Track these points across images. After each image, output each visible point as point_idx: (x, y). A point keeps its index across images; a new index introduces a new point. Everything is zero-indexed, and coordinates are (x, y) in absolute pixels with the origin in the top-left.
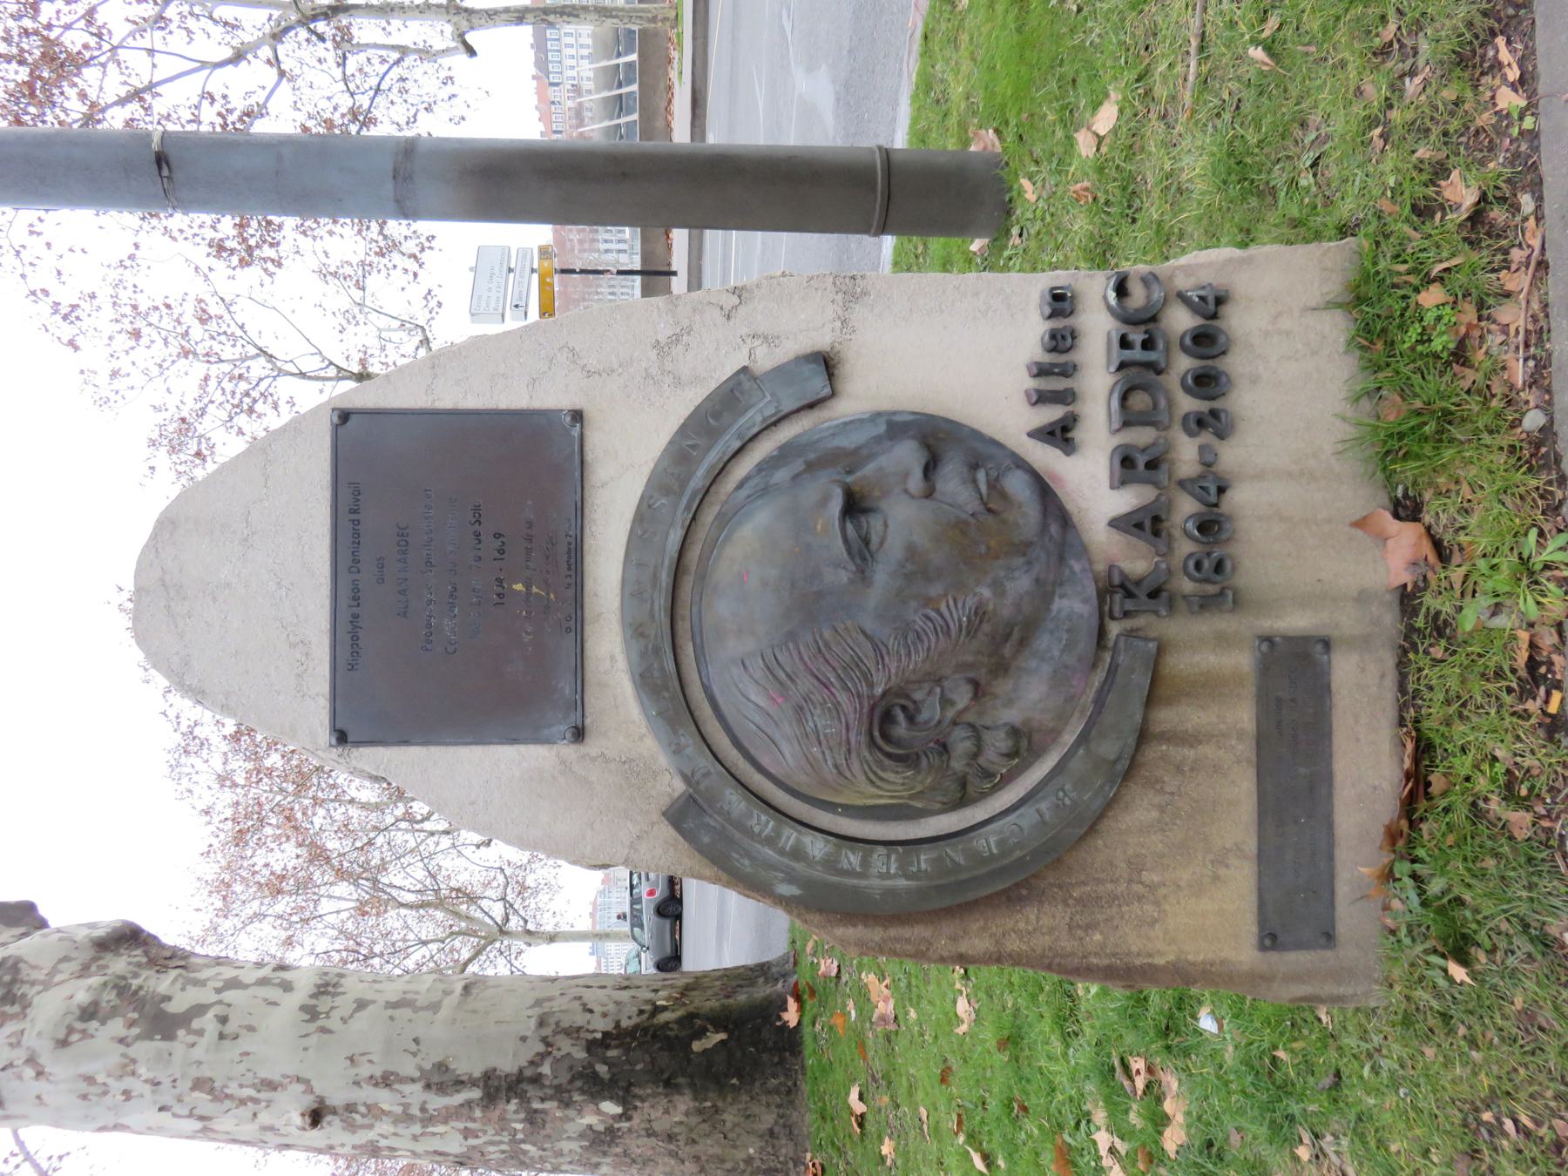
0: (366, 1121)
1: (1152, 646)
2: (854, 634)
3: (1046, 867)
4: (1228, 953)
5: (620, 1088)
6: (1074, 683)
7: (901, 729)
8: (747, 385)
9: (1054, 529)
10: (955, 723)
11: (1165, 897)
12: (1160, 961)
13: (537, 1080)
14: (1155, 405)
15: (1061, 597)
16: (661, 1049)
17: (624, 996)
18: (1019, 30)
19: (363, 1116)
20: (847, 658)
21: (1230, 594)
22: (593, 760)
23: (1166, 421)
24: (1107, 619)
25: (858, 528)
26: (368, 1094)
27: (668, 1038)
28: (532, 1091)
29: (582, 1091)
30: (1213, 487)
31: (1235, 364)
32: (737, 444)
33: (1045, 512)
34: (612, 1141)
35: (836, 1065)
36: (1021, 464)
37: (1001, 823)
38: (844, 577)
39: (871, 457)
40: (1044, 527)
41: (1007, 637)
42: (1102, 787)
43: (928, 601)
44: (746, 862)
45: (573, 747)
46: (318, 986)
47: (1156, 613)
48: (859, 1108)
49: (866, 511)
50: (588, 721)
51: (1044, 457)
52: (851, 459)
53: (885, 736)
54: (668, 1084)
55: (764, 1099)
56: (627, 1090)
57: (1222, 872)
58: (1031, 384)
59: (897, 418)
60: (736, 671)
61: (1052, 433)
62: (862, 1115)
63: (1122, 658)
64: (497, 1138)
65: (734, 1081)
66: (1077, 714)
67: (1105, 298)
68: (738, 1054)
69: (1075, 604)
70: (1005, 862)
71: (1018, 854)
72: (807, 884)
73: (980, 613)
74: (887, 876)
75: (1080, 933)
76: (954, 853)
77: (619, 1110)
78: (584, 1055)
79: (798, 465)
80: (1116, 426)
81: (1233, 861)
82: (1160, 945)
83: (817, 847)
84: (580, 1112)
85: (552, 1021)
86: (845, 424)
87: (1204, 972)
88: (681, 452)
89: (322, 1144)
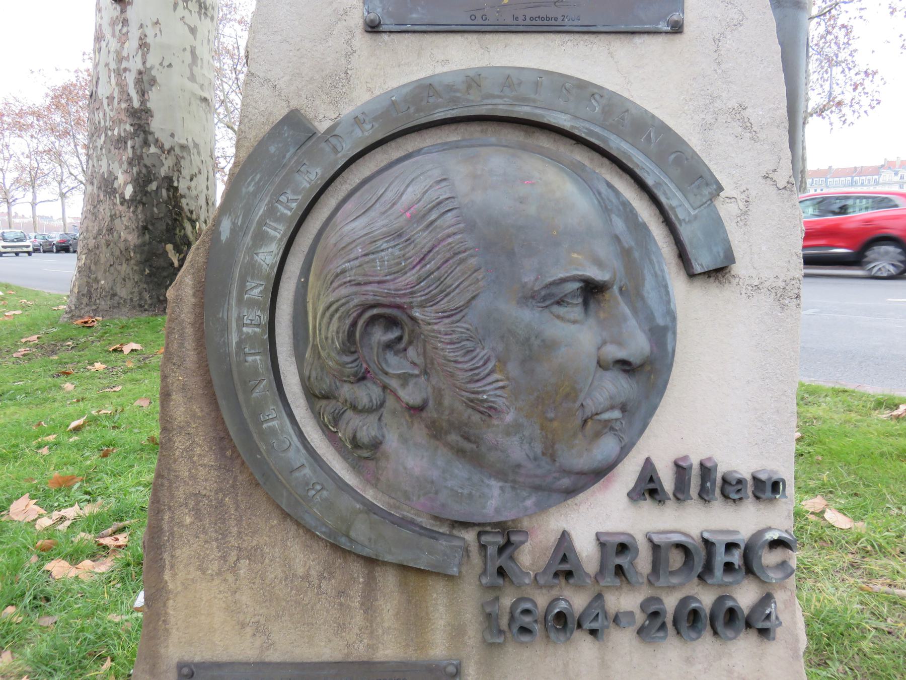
0: (117, 32)
1: (454, 571)
2: (472, 288)
3: (251, 474)
4: (175, 636)
5: (142, 197)
6: (422, 500)
7: (380, 336)
8: (706, 191)
9: (566, 482)
10: (385, 388)
11: (225, 580)
12: (167, 575)
13: (146, 143)
14: (672, 573)
15: (502, 488)
16: (168, 224)
17: (202, 201)
18: (882, 454)
19: (120, 31)
20: (448, 281)
21: (501, 640)
22: (348, 43)
23: (657, 584)
24: (478, 529)
25: (573, 294)
26: (134, 34)
27: (175, 229)
28: (139, 141)
29: (139, 173)
30: (595, 625)
31: (706, 644)
32: (650, 181)
33: (581, 473)
34: (107, 193)
35: (156, 335)
36: (625, 451)
37: (292, 432)
38: (528, 278)
39: (635, 311)
40: (566, 472)
41: (467, 438)
42: (324, 524)
43: (502, 361)
44: (251, 189)
45: (361, 23)
46: (205, 3)
47: (484, 572)
48: (127, 349)
49: (586, 304)
50: (385, 37)
51: (628, 473)
52: (633, 294)
53: (373, 320)
54: (145, 228)
55: (136, 290)
56: (140, 202)
57: (249, 631)
58: (695, 461)
59: (669, 336)
60: (437, 174)
61: (651, 480)
62: (122, 351)
63: (443, 543)
64: (108, 118)
65: (147, 271)
66: (392, 501)
67: (769, 529)
68: (165, 274)
69: (495, 501)
70: (255, 436)
71: (263, 447)
72: (232, 245)
73: (489, 411)
74: (241, 324)
75: (192, 503)
76: (263, 388)
77: (127, 197)
78: (163, 174)
79: (628, 241)
80: (656, 539)
81: (258, 642)
82: (181, 575)
83: (268, 256)
84: (126, 172)
85: (185, 154)
86: (666, 287)
87: (158, 614)
88: (644, 126)
89: (102, 5)
